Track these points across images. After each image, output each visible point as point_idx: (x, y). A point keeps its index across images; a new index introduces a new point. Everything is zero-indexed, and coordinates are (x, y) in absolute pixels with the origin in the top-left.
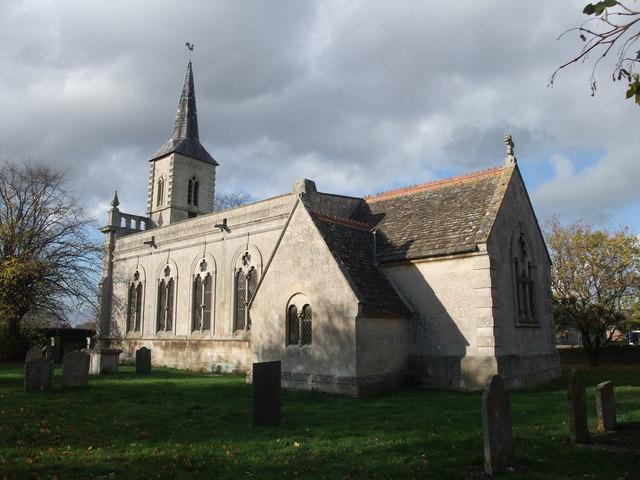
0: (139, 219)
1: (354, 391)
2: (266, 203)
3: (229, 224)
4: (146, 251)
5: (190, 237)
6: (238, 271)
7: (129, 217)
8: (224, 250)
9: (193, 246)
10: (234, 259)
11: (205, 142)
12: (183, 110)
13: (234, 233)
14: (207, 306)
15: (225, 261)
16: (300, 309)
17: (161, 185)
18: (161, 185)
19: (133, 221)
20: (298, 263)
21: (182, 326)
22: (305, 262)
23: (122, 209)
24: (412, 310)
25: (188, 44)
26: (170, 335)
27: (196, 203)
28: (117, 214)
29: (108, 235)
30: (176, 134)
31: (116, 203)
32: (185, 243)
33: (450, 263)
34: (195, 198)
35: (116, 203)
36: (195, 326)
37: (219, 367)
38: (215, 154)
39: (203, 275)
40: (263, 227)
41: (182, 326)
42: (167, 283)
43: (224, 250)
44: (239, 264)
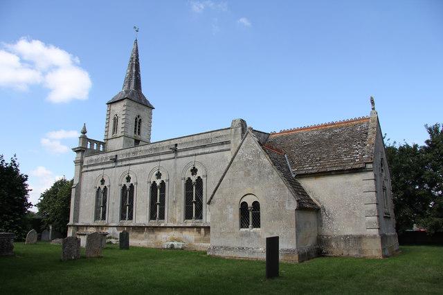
0: (99, 143)
1: (296, 257)
2: (210, 134)
3: (178, 148)
4: (111, 165)
5: (147, 156)
6: (152, 183)
7: (92, 141)
8: (175, 165)
9: (150, 162)
10: (150, 174)
11: (146, 91)
12: (131, 71)
13: (180, 154)
14: (97, 207)
15: (176, 173)
16: (250, 205)
17: (116, 120)
18: (116, 120)
19: (95, 144)
20: (248, 174)
21: (141, 216)
22: (254, 173)
23: (89, 135)
24: (319, 205)
25: (135, 27)
26: (132, 223)
27: (139, 133)
28: (84, 138)
29: (80, 154)
30: (127, 86)
31: (84, 132)
32: (143, 160)
33: (347, 176)
34: (139, 130)
35: (84, 132)
36: (152, 216)
37: (172, 245)
38: (152, 102)
39: (158, 182)
40: (207, 150)
41: (141, 216)
42: (128, 187)
43: (175, 165)
44: (189, 174)
